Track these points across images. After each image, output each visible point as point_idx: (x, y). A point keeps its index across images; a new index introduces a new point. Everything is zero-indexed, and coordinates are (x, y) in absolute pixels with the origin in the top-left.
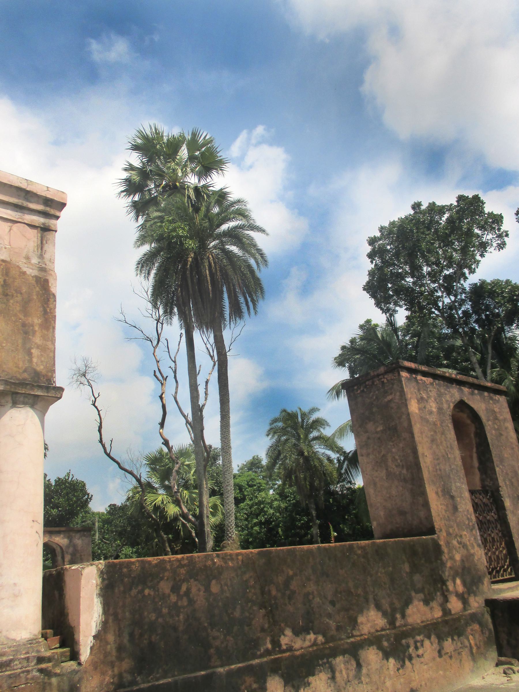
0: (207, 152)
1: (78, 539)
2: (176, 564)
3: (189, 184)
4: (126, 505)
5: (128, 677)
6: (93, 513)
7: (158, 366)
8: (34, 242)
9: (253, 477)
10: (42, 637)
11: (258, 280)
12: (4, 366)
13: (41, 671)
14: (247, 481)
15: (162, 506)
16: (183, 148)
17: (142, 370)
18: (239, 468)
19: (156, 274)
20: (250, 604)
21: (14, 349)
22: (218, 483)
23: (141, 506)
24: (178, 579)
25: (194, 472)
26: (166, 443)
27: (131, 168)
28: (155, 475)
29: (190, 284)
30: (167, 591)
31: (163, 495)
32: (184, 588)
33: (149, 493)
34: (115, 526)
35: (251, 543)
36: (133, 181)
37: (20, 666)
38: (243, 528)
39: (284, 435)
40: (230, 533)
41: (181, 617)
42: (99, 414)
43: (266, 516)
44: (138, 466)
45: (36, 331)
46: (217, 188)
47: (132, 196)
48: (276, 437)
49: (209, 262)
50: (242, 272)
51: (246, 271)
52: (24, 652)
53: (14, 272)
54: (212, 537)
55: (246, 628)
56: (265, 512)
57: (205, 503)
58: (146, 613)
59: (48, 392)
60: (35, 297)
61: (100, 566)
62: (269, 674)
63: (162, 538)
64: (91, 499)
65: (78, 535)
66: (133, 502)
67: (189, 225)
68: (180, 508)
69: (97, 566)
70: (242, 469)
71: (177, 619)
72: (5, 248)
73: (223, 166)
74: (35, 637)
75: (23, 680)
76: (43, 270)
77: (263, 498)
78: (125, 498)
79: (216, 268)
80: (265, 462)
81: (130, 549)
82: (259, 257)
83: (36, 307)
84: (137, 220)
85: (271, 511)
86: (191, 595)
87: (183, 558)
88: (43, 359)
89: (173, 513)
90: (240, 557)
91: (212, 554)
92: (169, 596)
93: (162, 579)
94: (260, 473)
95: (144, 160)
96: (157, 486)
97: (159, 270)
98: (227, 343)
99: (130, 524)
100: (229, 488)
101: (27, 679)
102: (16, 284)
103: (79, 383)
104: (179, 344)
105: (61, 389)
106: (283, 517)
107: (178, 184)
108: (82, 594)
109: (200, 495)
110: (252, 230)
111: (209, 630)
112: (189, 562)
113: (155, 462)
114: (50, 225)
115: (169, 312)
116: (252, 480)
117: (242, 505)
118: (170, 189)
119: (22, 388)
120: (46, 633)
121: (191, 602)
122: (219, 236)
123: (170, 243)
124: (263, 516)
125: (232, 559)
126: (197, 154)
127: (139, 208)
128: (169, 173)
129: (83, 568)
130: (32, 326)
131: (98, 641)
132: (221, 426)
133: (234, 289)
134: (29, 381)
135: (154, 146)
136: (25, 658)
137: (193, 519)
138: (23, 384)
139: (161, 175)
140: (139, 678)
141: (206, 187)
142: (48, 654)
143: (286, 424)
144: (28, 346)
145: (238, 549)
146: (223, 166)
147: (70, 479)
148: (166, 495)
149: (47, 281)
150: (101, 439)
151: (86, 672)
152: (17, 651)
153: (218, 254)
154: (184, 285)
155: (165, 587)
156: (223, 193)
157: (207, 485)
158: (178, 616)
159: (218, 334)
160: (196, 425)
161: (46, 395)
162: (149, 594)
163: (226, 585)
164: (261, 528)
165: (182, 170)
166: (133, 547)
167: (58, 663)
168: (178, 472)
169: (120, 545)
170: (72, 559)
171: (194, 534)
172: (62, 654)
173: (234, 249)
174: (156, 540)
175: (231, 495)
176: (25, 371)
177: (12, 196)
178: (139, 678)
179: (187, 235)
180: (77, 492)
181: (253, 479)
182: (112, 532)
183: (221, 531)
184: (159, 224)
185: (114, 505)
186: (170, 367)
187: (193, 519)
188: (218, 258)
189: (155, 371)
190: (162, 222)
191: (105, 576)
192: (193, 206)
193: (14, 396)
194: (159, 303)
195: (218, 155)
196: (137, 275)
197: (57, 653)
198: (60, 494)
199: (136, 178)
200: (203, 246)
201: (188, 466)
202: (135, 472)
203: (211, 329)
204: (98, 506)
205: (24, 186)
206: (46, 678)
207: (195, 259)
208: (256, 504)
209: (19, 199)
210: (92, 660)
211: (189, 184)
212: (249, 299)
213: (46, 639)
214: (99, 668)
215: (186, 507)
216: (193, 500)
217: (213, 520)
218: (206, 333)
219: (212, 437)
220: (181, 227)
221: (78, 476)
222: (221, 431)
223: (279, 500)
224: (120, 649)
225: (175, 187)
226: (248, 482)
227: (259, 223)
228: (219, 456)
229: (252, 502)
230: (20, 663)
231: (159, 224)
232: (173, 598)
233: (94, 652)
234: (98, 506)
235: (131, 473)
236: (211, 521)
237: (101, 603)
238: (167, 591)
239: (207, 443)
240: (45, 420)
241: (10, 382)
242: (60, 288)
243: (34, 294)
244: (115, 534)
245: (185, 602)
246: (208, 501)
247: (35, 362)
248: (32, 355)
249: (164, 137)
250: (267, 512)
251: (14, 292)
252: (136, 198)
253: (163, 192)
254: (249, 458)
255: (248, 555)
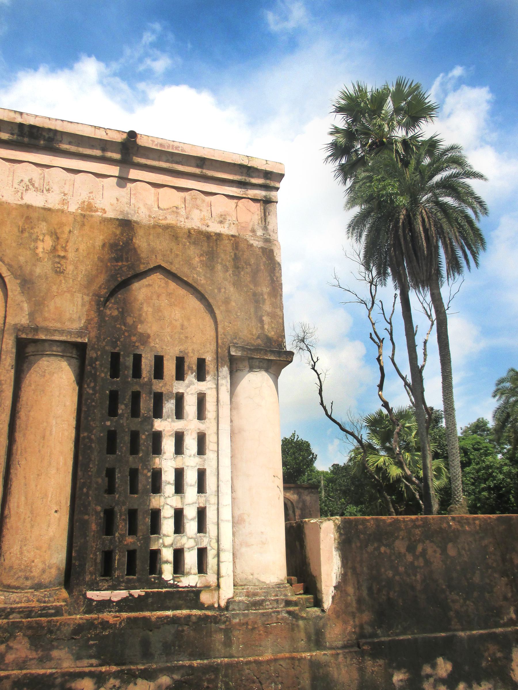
0: (413, 100)
1: (307, 495)
2: (410, 525)
3: (396, 138)
4: (349, 466)
5: (368, 629)
6: (318, 472)
7: (374, 329)
8: (258, 215)
9: (478, 440)
10: (288, 582)
11: (478, 230)
12: (241, 334)
13: (289, 613)
14: (472, 444)
15: (384, 467)
16: (388, 101)
17: (353, 336)
18: (462, 431)
19: (367, 236)
20: (490, 571)
21: (247, 317)
22: (441, 446)
23: (363, 466)
24: (413, 539)
25: (416, 434)
26: (386, 405)
27: (336, 131)
28: (376, 437)
29: (403, 243)
30: (403, 550)
31: (385, 456)
32: (420, 548)
33: (371, 454)
34: (339, 485)
35: (479, 508)
36: (339, 144)
37: (271, 606)
38: (469, 493)
39: (513, 396)
40: (457, 497)
41: (418, 577)
42: (319, 378)
43: (495, 482)
44: (358, 427)
45: (265, 299)
46: (426, 137)
47: (339, 160)
48: (504, 398)
49: (422, 217)
50: (459, 224)
51: (464, 223)
52: (273, 594)
53: (242, 245)
54: (437, 500)
55: (487, 595)
56: (494, 478)
57: (429, 465)
58: (383, 570)
59: (279, 357)
60: (262, 268)
61: (337, 521)
62: (514, 645)
63: (386, 498)
64: (315, 458)
65: (306, 492)
66: (355, 462)
67: (399, 181)
68: (403, 469)
69: (334, 521)
70: (465, 432)
71: (414, 578)
72: (234, 224)
73: (432, 113)
74: (282, 582)
75: (275, 620)
76: (267, 241)
77: (491, 462)
78: (348, 458)
79: (430, 223)
80: (491, 424)
81: (355, 507)
82: (478, 206)
83: (264, 277)
84: (345, 183)
85: (501, 477)
86: (427, 556)
87: (417, 518)
88: (273, 325)
89: (395, 474)
90: (477, 522)
91: (447, 517)
92: (405, 555)
93: (397, 538)
94: (487, 436)
95: (348, 121)
96: (378, 447)
97: (370, 231)
98: (445, 301)
99: (353, 483)
100: (454, 451)
101: (278, 619)
102: (245, 256)
103: (298, 348)
104: (394, 305)
105: (291, 354)
106: (515, 483)
107: (384, 140)
108: (322, 546)
109: (424, 457)
110: (467, 177)
111: (448, 593)
112: (424, 523)
113: (376, 423)
114: (271, 197)
115: (382, 274)
116: (478, 443)
117: (467, 469)
118: (377, 146)
119: (257, 353)
120: (291, 579)
121: (428, 563)
122: (431, 189)
123: (380, 203)
124: (492, 481)
125: (468, 524)
126: (402, 105)
127: (346, 171)
128: (375, 130)
129: (321, 522)
130: (262, 294)
131: (339, 592)
132: (443, 387)
133: (451, 243)
134: (263, 347)
135: (358, 105)
136: (275, 600)
137: (417, 482)
138: (257, 349)
139: (367, 133)
140: (379, 632)
141: (414, 138)
142: (295, 598)
143: (515, 384)
144: (259, 314)
145: (464, 513)
146: (432, 113)
147: (295, 440)
148: (388, 456)
149: (272, 251)
150: (322, 401)
151: (329, 619)
152: (267, 593)
153: (432, 208)
154: (397, 245)
155: (400, 546)
156: (433, 141)
157: (431, 448)
158: (416, 576)
159: (435, 291)
160: (416, 387)
161: (278, 359)
162: (385, 551)
163: (464, 549)
164: (490, 493)
165: (388, 124)
166: (357, 506)
167: (303, 608)
168: (398, 433)
169: (344, 504)
170: (302, 514)
171: (418, 497)
172: (307, 600)
173: (449, 200)
174: (380, 500)
175: (457, 459)
176: (258, 337)
177: (236, 175)
178: (379, 632)
179: (397, 192)
180: (302, 452)
181: (479, 442)
182: (337, 490)
183: (447, 496)
184: (368, 184)
185: (337, 465)
186: (386, 329)
187: (417, 482)
188: (432, 213)
189: (371, 334)
190: (371, 181)
191: (342, 531)
192: (401, 160)
193: (251, 361)
194: (372, 265)
195: (427, 101)
196: (349, 238)
197: (302, 599)
198: (288, 453)
199: (342, 140)
200: (415, 201)
201: (409, 428)
202: (356, 434)
203: (427, 287)
204: (322, 465)
205: (245, 162)
206: (294, 619)
207: (408, 216)
208: (484, 468)
209: (242, 176)
210: (334, 608)
211: (396, 138)
212: (468, 252)
213: (291, 585)
214: (341, 616)
215: (409, 469)
216: (415, 462)
217: (437, 483)
218: (422, 291)
219: (434, 398)
220: (390, 185)
221: (303, 436)
222: (443, 393)
223: (509, 466)
224: (360, 601)
225: (382, 143)
226: (473, 446)
227: (476, 168)
228: (442, 418)
229: (479, 466)
230: (271, 604)
231: (368, 184)
232: (410, 558)
233: (335, 602)
234: (322, 465)
235: (352, 434)
236: (435, 484)
237: (339, 556)
238: (403, 550)
239: (428, 405)
240: (417, 353)
241: (247, 348)
242: (284, 256)
243: (262, 264)
244: (340, 493)
245: (421, 562)
246: (432, 464)
247: (267, 328)
248: (263, 322)
249: (368, 93)
250: (496, 477)
251: (244, 264)
252: (343, 161)
253: (369, 151)
254: (474, 420)
255: (485, 520)
